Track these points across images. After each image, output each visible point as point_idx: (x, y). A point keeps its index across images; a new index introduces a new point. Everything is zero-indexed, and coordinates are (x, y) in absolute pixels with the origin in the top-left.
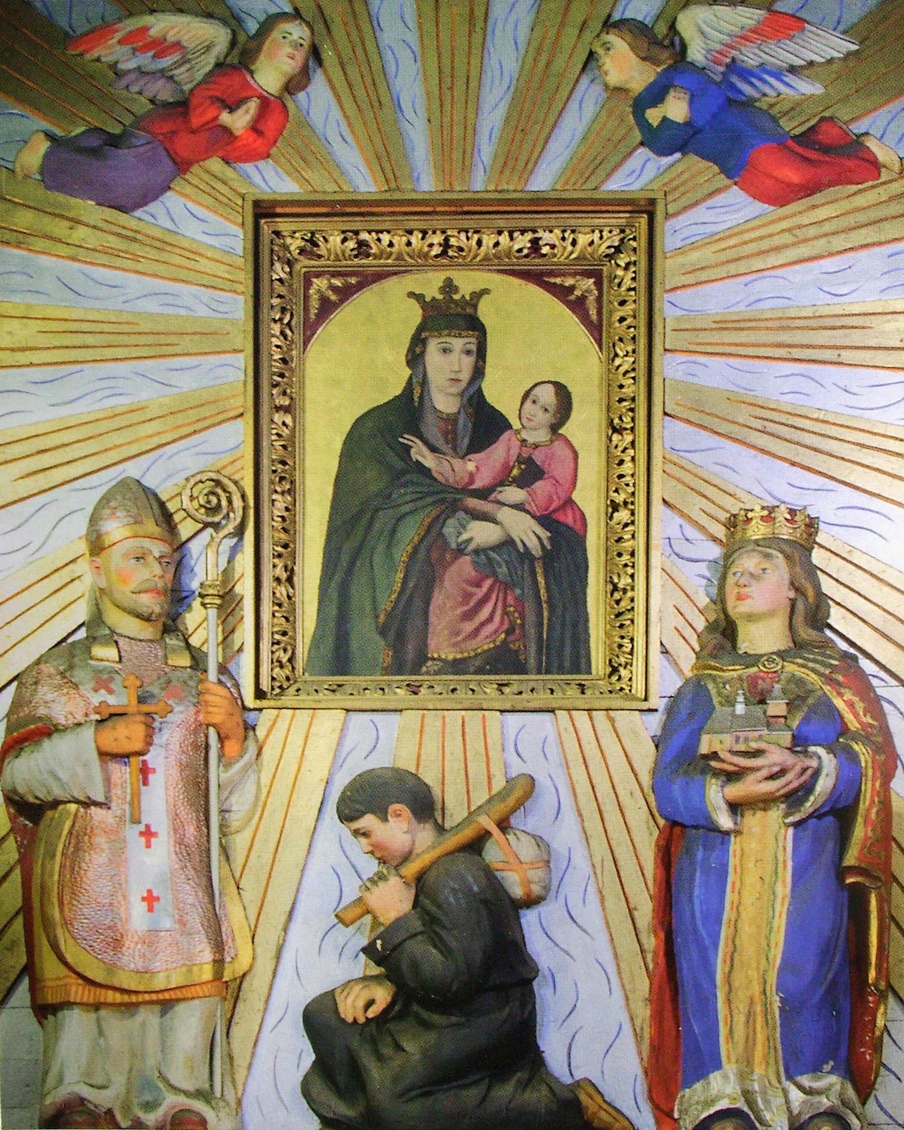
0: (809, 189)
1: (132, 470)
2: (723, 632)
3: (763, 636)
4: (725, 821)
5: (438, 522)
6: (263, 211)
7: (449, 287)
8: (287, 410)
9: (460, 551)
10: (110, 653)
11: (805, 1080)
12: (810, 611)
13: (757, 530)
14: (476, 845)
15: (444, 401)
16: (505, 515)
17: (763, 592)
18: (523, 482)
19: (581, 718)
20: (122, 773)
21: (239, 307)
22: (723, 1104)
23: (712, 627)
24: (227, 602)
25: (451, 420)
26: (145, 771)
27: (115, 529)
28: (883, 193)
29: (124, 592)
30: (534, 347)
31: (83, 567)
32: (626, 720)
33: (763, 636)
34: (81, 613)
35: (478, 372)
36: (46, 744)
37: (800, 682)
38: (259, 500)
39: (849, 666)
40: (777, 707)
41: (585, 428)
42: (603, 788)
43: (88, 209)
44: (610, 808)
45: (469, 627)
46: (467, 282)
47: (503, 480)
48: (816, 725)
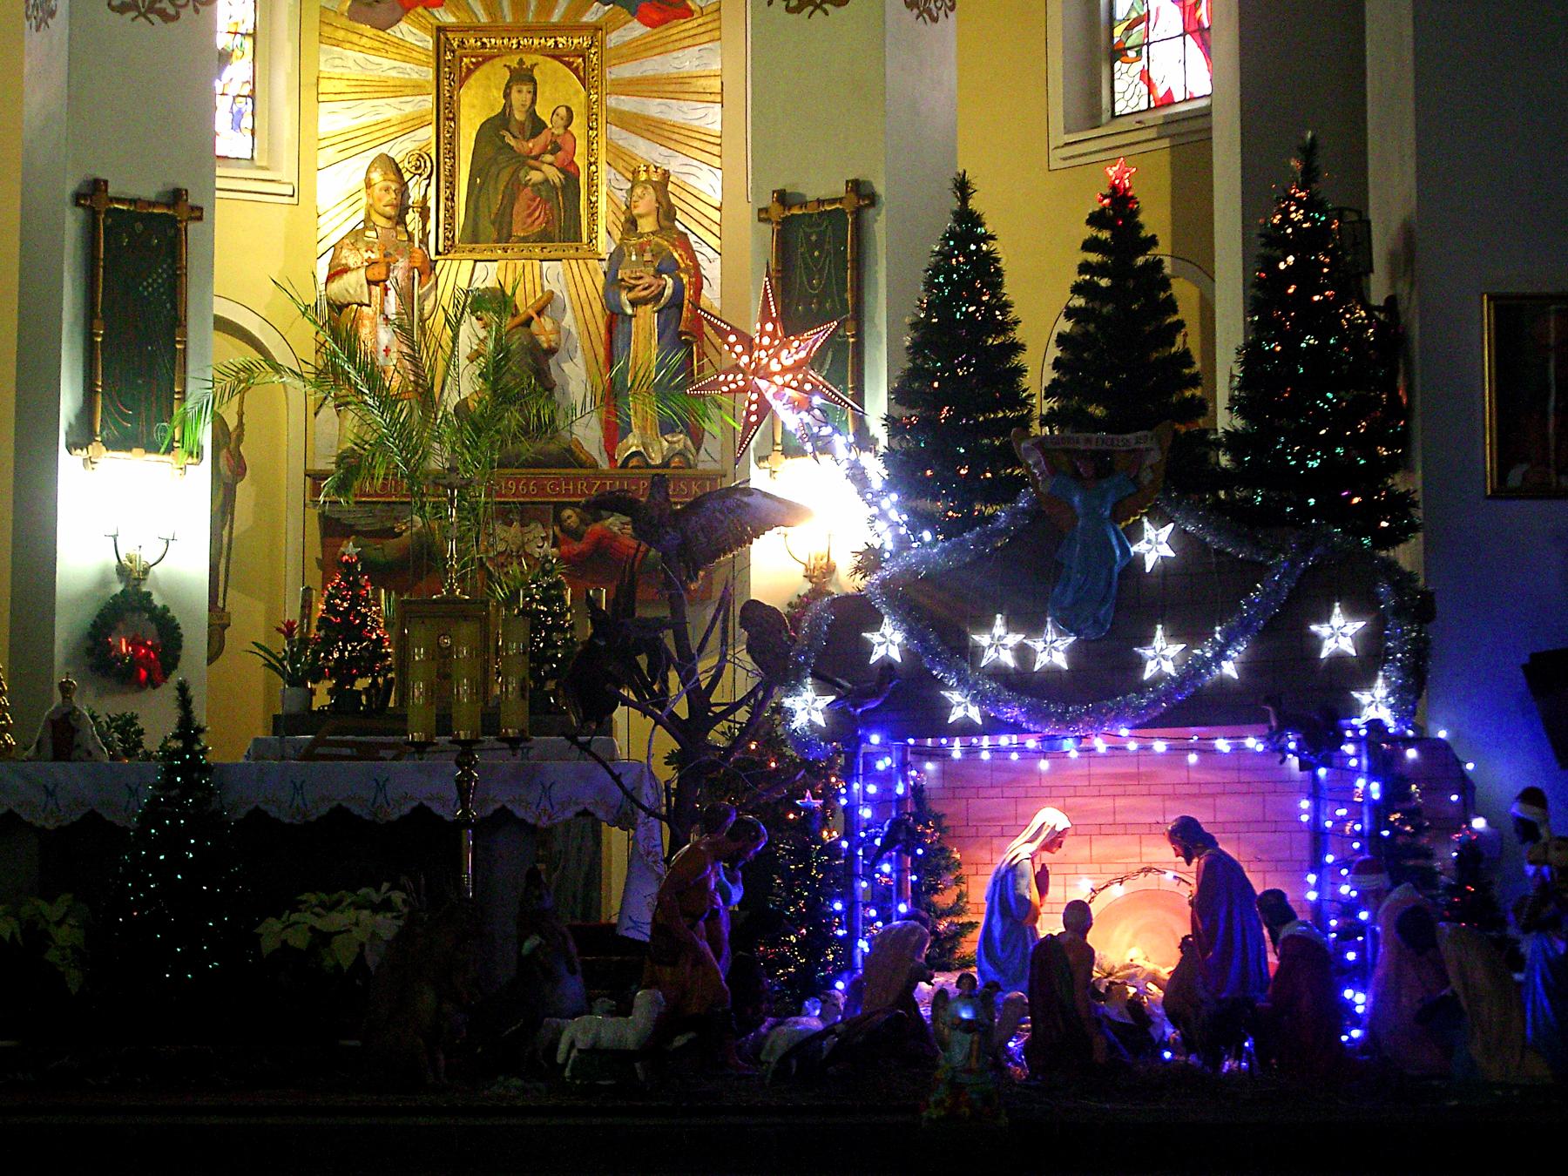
0: (664, 21)
1: (384, 149)
2: (632, 223)
3: (647, 225)
4: (629, 311)
5: (516, 171)
6: (441, 30)
7: (521, 62)
8: (452, 119)
9: (526, 185)
10: (373, 234)
11: (668, 437)
12: (667, 213)
13: (643, 177)
14: (528, 322)
15: (519, 116)
16: (545, 167)
17: (646, 203)
18: (553, 153)
19: (573, 263)
20: (377, 290)
21: (430, 74)
22: (634, 449)
23: (627, 221)
24: (424, 214)
25: (522, 124)
26: (386, 289)
27: (377, 177)
28: (695, 23)
29: (380, 206)
30: (557, 91)
31: (363, 194)
32: (593, 263)
33: (647, 225)
34: (361, 215)
35: (534, 102)
36: (345, 276)
37: (657, 244)
38: (440, 164)
39: (683, 241)
40: (648, 257)
41: (578, 127)
42: (583, 297)
43: (367, 29)
44: (586, 306)
45: (530, 221)
46: (529, 60)
47: (544, 152)
48: (666, 266)
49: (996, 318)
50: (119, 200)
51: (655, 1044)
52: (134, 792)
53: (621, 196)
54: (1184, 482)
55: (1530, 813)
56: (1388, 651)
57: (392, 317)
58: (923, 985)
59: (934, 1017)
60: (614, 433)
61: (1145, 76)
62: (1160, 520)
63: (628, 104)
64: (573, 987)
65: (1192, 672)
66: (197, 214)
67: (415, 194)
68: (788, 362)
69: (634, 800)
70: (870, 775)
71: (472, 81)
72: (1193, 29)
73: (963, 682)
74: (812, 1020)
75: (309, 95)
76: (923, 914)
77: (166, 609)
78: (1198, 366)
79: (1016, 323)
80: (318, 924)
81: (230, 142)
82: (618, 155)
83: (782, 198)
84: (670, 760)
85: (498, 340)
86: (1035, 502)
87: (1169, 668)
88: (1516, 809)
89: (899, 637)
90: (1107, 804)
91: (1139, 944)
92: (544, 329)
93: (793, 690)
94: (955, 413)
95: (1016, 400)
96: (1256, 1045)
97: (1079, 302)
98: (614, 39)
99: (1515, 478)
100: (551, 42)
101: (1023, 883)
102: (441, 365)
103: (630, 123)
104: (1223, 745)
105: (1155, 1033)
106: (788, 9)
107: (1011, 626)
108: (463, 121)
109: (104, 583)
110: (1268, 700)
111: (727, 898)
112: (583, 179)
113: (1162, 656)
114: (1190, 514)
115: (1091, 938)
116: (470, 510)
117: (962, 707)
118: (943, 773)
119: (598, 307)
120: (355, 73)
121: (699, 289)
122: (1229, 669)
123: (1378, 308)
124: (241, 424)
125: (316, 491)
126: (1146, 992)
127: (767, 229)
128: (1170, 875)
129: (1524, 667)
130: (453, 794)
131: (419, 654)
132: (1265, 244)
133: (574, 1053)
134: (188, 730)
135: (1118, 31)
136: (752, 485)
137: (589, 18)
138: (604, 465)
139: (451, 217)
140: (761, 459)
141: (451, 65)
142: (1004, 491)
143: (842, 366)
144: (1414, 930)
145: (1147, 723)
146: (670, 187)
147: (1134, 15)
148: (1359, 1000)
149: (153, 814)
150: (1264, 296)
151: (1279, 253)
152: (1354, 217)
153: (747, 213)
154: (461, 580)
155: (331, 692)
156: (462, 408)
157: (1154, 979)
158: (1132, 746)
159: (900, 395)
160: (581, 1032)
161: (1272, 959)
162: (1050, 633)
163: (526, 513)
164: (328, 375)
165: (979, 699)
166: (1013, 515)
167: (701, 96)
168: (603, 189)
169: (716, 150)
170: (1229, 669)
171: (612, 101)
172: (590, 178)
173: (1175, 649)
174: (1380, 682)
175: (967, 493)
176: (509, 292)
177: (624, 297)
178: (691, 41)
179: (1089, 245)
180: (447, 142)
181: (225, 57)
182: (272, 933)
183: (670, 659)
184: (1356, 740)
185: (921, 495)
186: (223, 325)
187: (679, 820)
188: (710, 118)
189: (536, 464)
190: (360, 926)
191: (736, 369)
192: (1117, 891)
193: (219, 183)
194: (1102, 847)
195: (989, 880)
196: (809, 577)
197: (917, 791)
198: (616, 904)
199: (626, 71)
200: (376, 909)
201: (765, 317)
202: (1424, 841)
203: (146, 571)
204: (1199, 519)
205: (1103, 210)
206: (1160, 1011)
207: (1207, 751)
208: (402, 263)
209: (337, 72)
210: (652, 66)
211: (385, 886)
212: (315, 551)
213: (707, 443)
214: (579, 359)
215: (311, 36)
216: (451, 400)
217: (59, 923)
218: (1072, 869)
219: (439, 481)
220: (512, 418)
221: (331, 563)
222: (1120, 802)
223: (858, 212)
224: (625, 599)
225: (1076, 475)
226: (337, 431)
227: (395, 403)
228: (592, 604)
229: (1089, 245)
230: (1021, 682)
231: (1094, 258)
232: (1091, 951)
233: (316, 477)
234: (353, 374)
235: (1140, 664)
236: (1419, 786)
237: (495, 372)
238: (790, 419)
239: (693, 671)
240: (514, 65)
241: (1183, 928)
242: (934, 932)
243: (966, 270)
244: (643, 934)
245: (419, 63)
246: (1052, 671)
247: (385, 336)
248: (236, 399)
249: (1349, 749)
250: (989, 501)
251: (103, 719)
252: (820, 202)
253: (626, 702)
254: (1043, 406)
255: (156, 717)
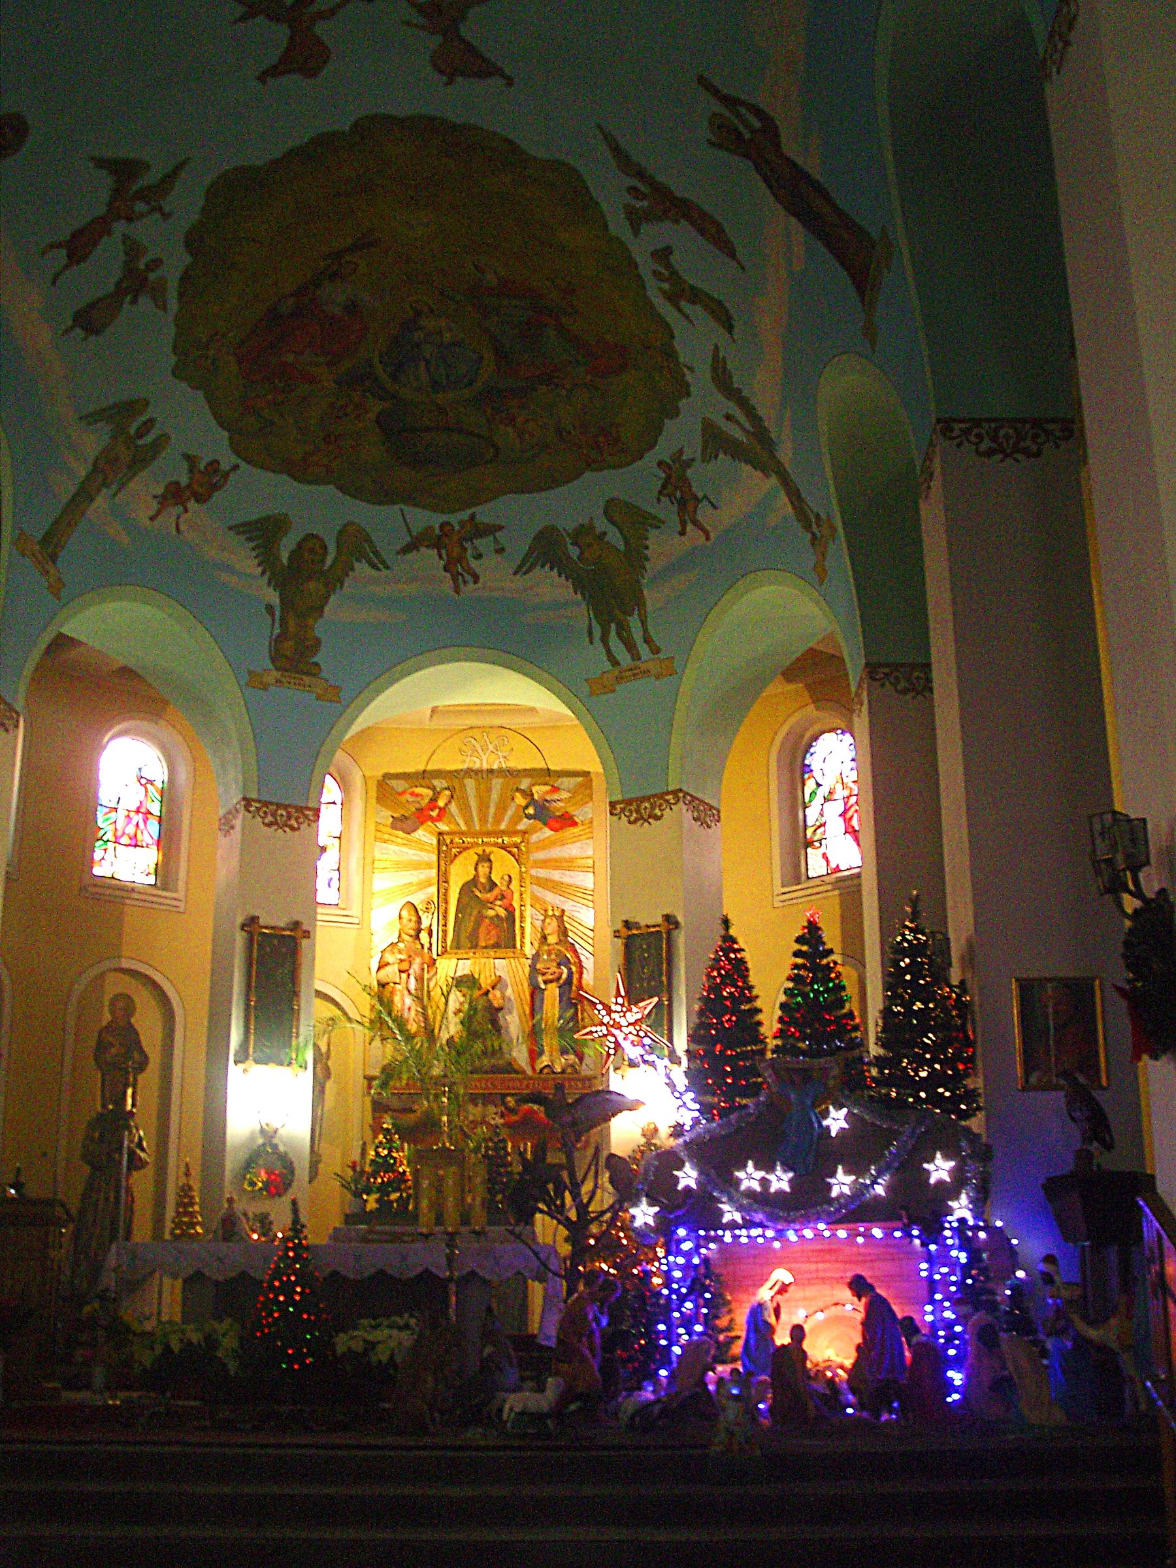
0: (562, 828)
3: (552, 939)
4: (543, 986)
12: (563, 932)
13: (550, 913)
15: (483, 880)
17: (552, 926)
20: (404, 976)
21: (435, 858)
24: (430, 934)
27: (405, 914)
29: (406, 930)
30: (503, 866)
40: (553, 957)
49: (745, 994)
50: (266, 928)
51: (558, 1412)
52: (265, 1260)
53: (538, 924)
54: (851, 1087)
55: (1048, 1268)
56: (968, 1179)
57: (413, 991)
58: (711, 1373)
59: (717, 1390)
60: (534, 1055)
61: (824, 856)
62: (839, 1107)
63: (543, 873)
64: (512, 1375)
65: (859, 1191)
66: (307, 934)
67: (425, 924)
68: (632, 1020)
69: (545, 1266)
70: (679, 1253)
71: (457, 861)
72: (850, 830)
73: (731, 1200)
74: (648, 1393)
75: (368, 869)
76: (710, 1332)
77: (286, 1153)
78: (857, 1020)
79: (757, 997)
80: (370, 1337)
81: (325, 894)
82: (536, 899)
83: (627, 924)
84: (566, 1240)
85: (470, 1004)
86: (768, 1097)
87: (846, 1190)
88: (1043, 1267)
89: (694, 1174)
90: (813, 1267)
91: (833, 1348)
92: (496, 997)
93: (635, 1204)
94: (724, 1048)
95: (759, 1040)
96: (899, 1405)
97: (791, 985)
98: (534, 838)
99: (1033, 1079)
100: (500, 840)
101: (766, 1313)
102: (439, 1018)
103: (538, 882)
104: (877, 1233)
105: (842, 1398)
106: (630, 822)
107: (757, 1167)
108: (451, 882)
109: (252, 1138)
110: (901, 1208)
111: (599, 1324)
112: (517, 914)
113: (842, 1183)
114: (855, 1104)
115: (806, 1345)
116: (454, 1097)
117: (730, 1214)
118: (720, 1250)
119: (526, 985)
120: (394, 857)
121: (581, 974)
122: (879, 1190)
123: (956, 987)
124: (329, 1049)
125: (370, 1087)
126: (835, 1375)
127: (619, 941)
128: (849, 1307)
129: (1043, 1185)
130: (443, 1261)
131: (425, 1183)
132: (892, 953)
133: (513, 1415)
134: (297, 1227)
135: (809, 832)
136: (611, 1089)
137: (521, 827)
138: (529, 1072)
139: (445, 932)
140: (616, 1069)
141: (446, 853)
142: (753, 1090)
143: (662, 1019)
144: (987, 1337)
145: (834, 1221)
146: (565, 918)
147: (818, 824)
148: (957, 1377)
149: (277, 1273)
150: (893, 981)
151: (900, 957)
152: (939, 936)
153: (609, 933)
154: (450, 1138)
155: (377, 1201)
156: (450, 1041)
157: (842, 1367)
158: (827, 1234)
159: (693, 1038)
160: (516, 1402)
161: (907, 1354)
162: (779, 1170)
163: (487, 1099)
164: (377, 1023)
165: (740, 1208)
166: (757, 1104)
167: (584, 869)
168: (528, 920)
169: (590, 898)
170: (879, 1190)
171: (533, 872)
172: (521, 912)
173: (850, 1179)
174: (963, 1196)
175: (730, 1093)
176: (476, 976)
177: (540, 979)
178: (576, 839)
179: (797, 954)
180: (443, 896)
181: (323, 849)
182: (343, 1342)
183: (566, 1187)
184: (951, 1229)
185: (705, 1093)
186: (319, 994)
187: (572, 1277)
188: (588, 881)
189: (492, 1072)
190: (390, 1338)
191: (602, 1024)
192: (820, 1316)
193: (319, 917)
194: (810, 1291)
195: (747, 1311)
196: (644, 1135)
197: (705, 1261)
198: (536, 1326)
199: (541, 855)
200: (400, 1328)
201: (618, 995)
202: (991, 1285)
203: (276, 1131)
204: (861, 1105)
205: (804, 934)
206: (845, 1386)
207: (868, 1236)
208: (418, 960)
209: (385, 857)
210: (556, 852)
211: (406, 1316)
212: (369, 1118)
213: (586, 1061)
214: (515, 1013)
215: (370, 838)
216: (444, 1036)
217: (224, 1335)
218: (793, 1304)
219: (438, 1082)
220: (478, 1046)
221: (377, 1128)
222: (821, 1266)
223: (669, 932)
224: (540, 1151)
225: (793, 1082)
226: (384, 1052)
227: (413, 1038)
228: (522, 1155)
229: (797, 954)
230: (763, 1199)
231: (800, 961)
232: (804, 1353)
233: (370, 1079)
234: (390, 1023)
235: (829, 1187)
236: (989, 1257)
237: (467, 1022)
238: (633, 1052)
239: (579, 1194)
240: (481, 852)
241: (859, 1340)
242: (717, 1342)
243: (730, 968)
244: (552, 1343)
245: (429, 852)
246: (780, 1192)
247: (408, 1001)
248: (326, 1036)
249: (947, 1233)
250: (744, 1096)
251: (251, 1215)
252: (648, 926)
253: (541, 1211)
254: (772, 1043)
255: (280, 1213)
